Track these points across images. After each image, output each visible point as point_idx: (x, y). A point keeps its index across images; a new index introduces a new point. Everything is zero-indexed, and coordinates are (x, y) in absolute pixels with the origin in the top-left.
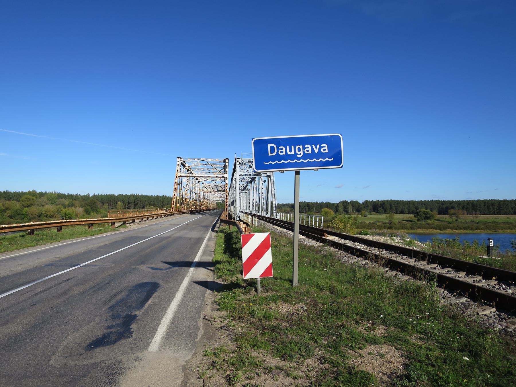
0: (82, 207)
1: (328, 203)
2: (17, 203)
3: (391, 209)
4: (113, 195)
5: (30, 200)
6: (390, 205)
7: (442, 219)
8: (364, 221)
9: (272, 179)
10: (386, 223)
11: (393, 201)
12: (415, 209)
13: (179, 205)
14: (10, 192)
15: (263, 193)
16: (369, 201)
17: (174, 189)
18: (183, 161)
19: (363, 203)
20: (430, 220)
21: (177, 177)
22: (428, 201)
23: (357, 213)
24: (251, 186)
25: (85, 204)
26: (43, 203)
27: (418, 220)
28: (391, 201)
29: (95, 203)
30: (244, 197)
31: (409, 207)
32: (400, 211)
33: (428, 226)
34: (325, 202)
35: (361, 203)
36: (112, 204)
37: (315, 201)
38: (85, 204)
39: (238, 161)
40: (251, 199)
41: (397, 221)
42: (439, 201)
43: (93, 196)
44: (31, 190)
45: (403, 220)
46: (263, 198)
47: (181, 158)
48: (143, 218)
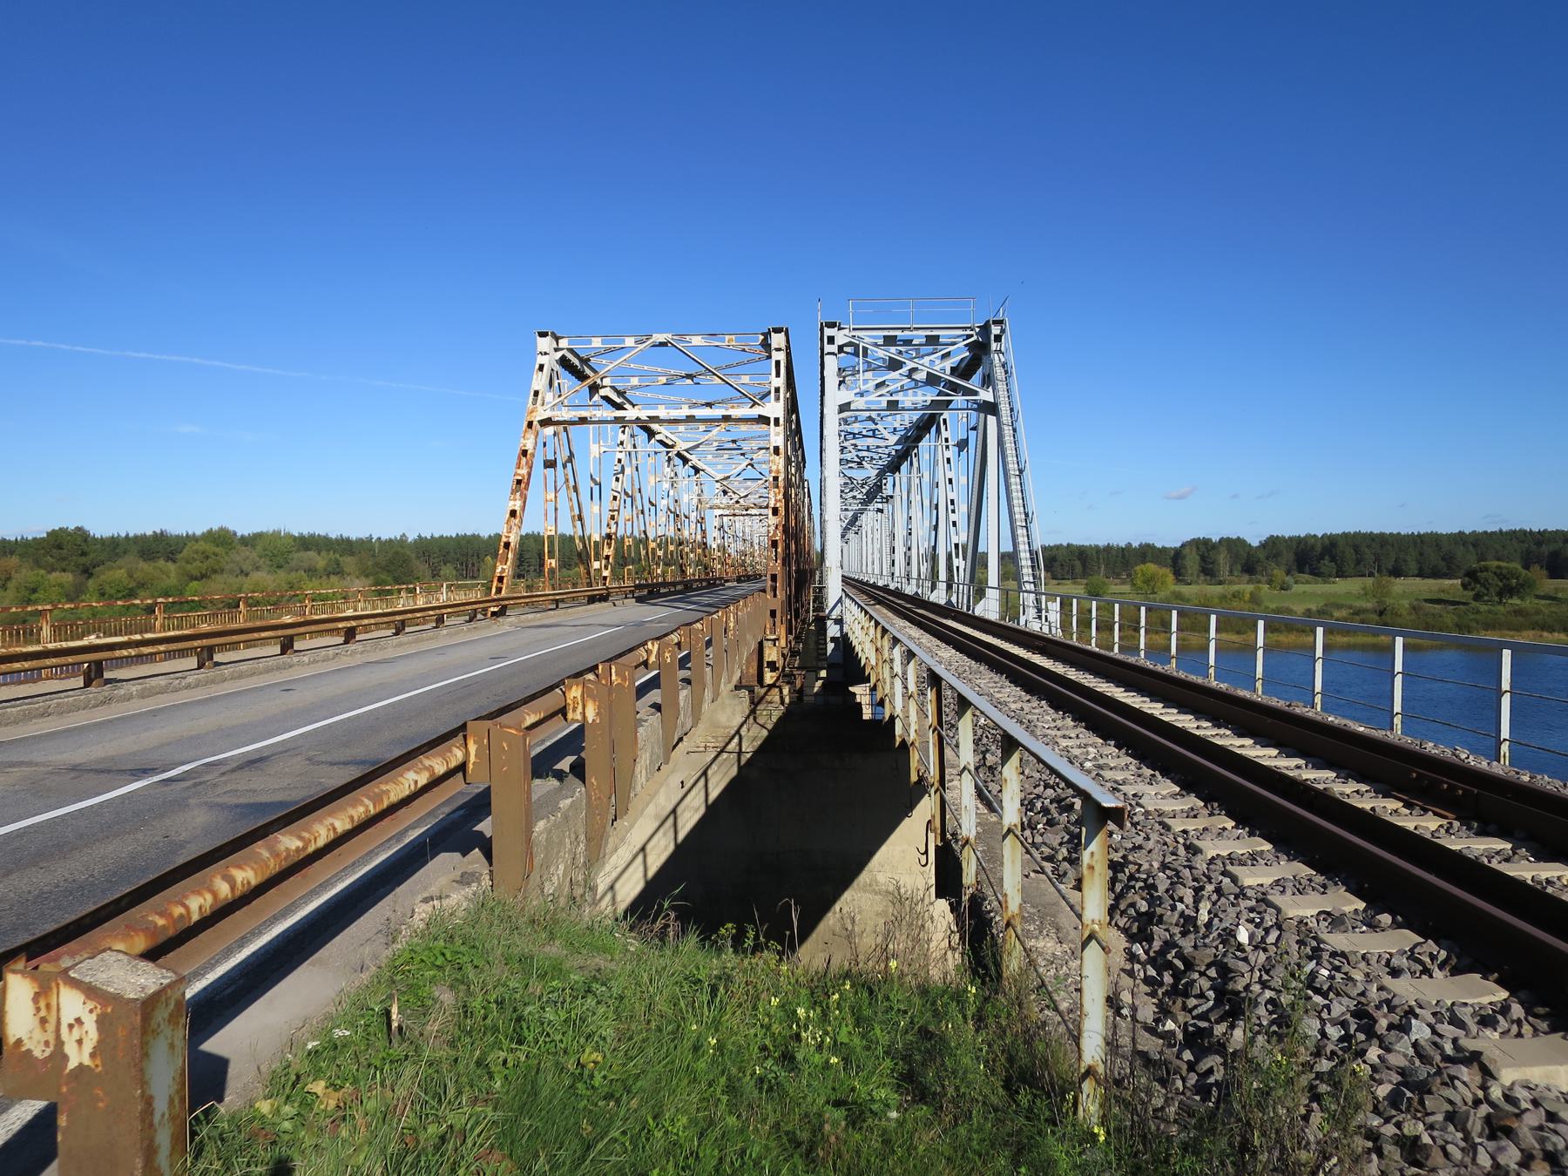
0: (367, 576)
1: (1148, 545)
2: (170, 565)
3: (1358, 562)
4: (476, 537)
5: (207, 557)
6: (1356, 549)
7: (1560, 595)
8: (1286, 605)
9: (1006, 418)
10: (1365, 611)
11: (1365, 534)
12: (1443, 559)
13: (553, 561)
14: (177, 536)
15: (952, 502)
16: (1283, 537)
17: (511, 484)
18: (568, 349)
19: (1264, 545)
20: (1522, 599)
21: (530, 424)
22: (1486, 532)
23: (1246, 577)
24: (895, 485)
25: (376, 564)
26: (247, 567)
27: (1477, 597)
28: (1357, 535)
29: (404, 561)
30: (872, 528)
31: (1421, 554)
32: (1390, 567)
33: (1521, 619)
34: (1135, 544)
35: (1255, 543)
36: (473, 565)
37: (1102, 543)
38: (376, 564)
39: (831, 340)
40: (900, 533)
41: (1406, 603)
42: (1523, 532)
43: (415, 540)
44: (215, 528)
45: (1426, 601)
46: (954, 524)
47: (557, 339)
48: (210, 650)
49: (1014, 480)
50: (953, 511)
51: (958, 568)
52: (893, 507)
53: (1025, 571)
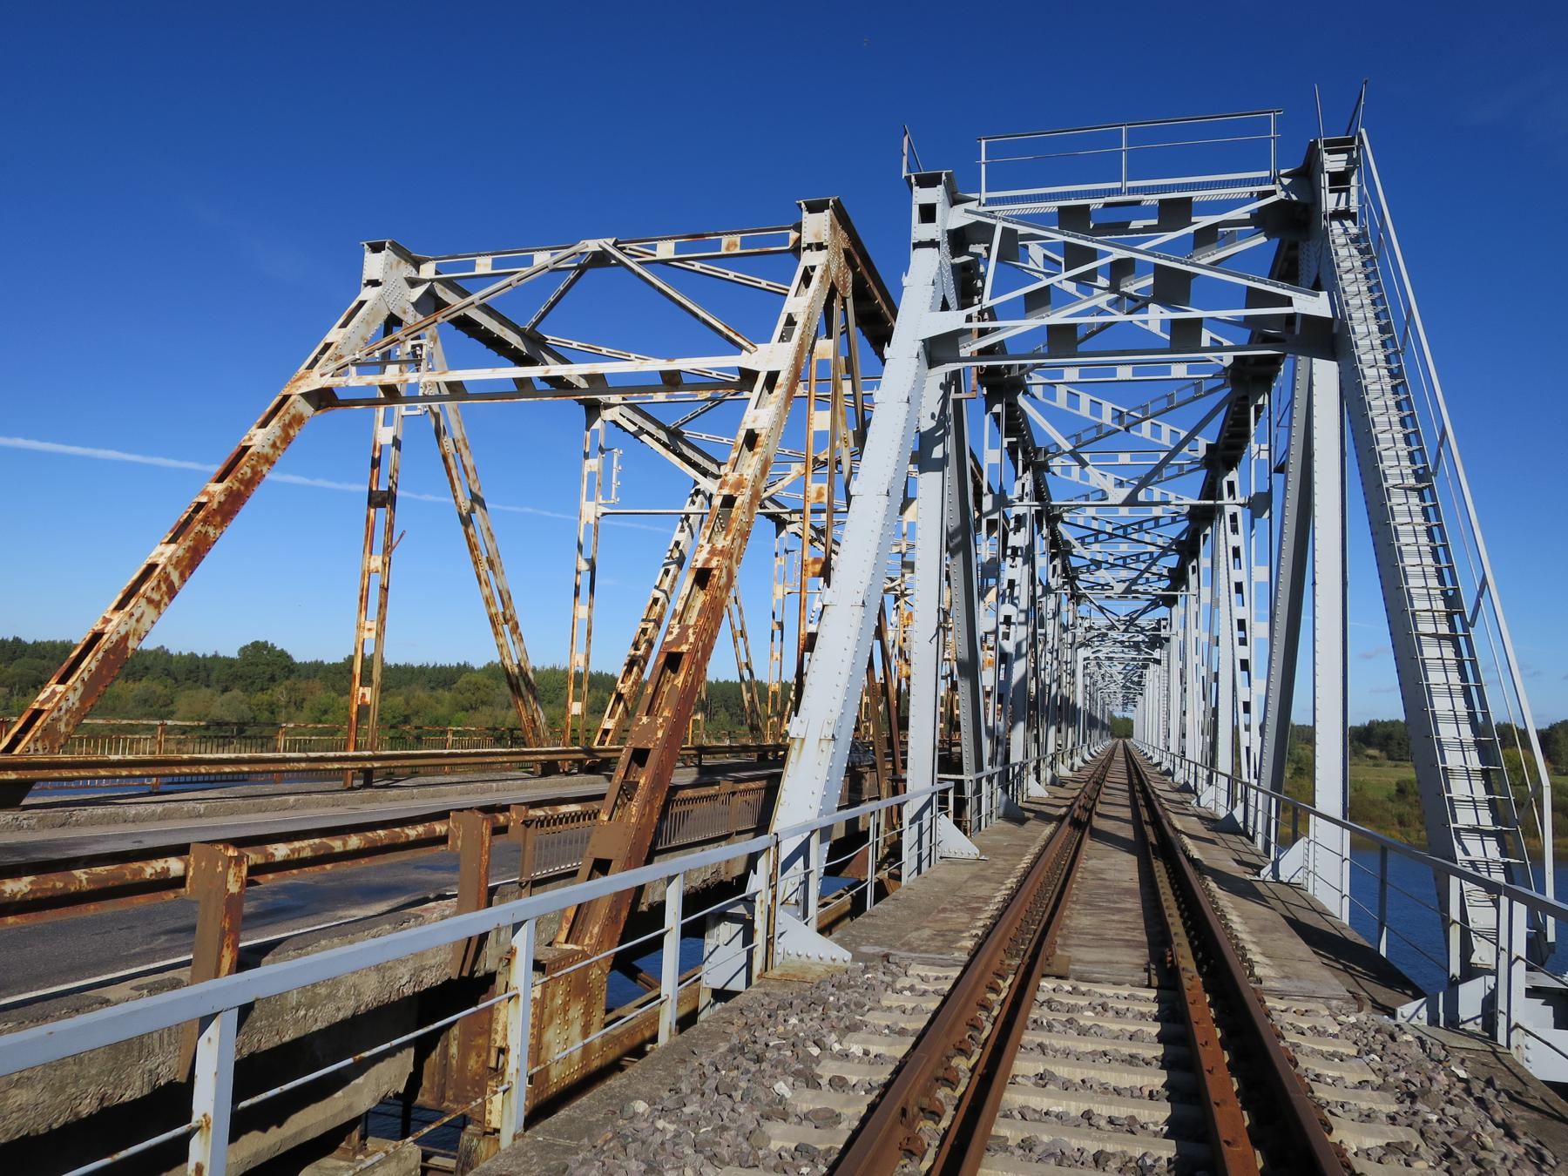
13: (368, 691)
49: (1405, 510)
50: (1243, 642)
51: (1248, 749)
52: (1169, 654)
53: (1458, 788)
